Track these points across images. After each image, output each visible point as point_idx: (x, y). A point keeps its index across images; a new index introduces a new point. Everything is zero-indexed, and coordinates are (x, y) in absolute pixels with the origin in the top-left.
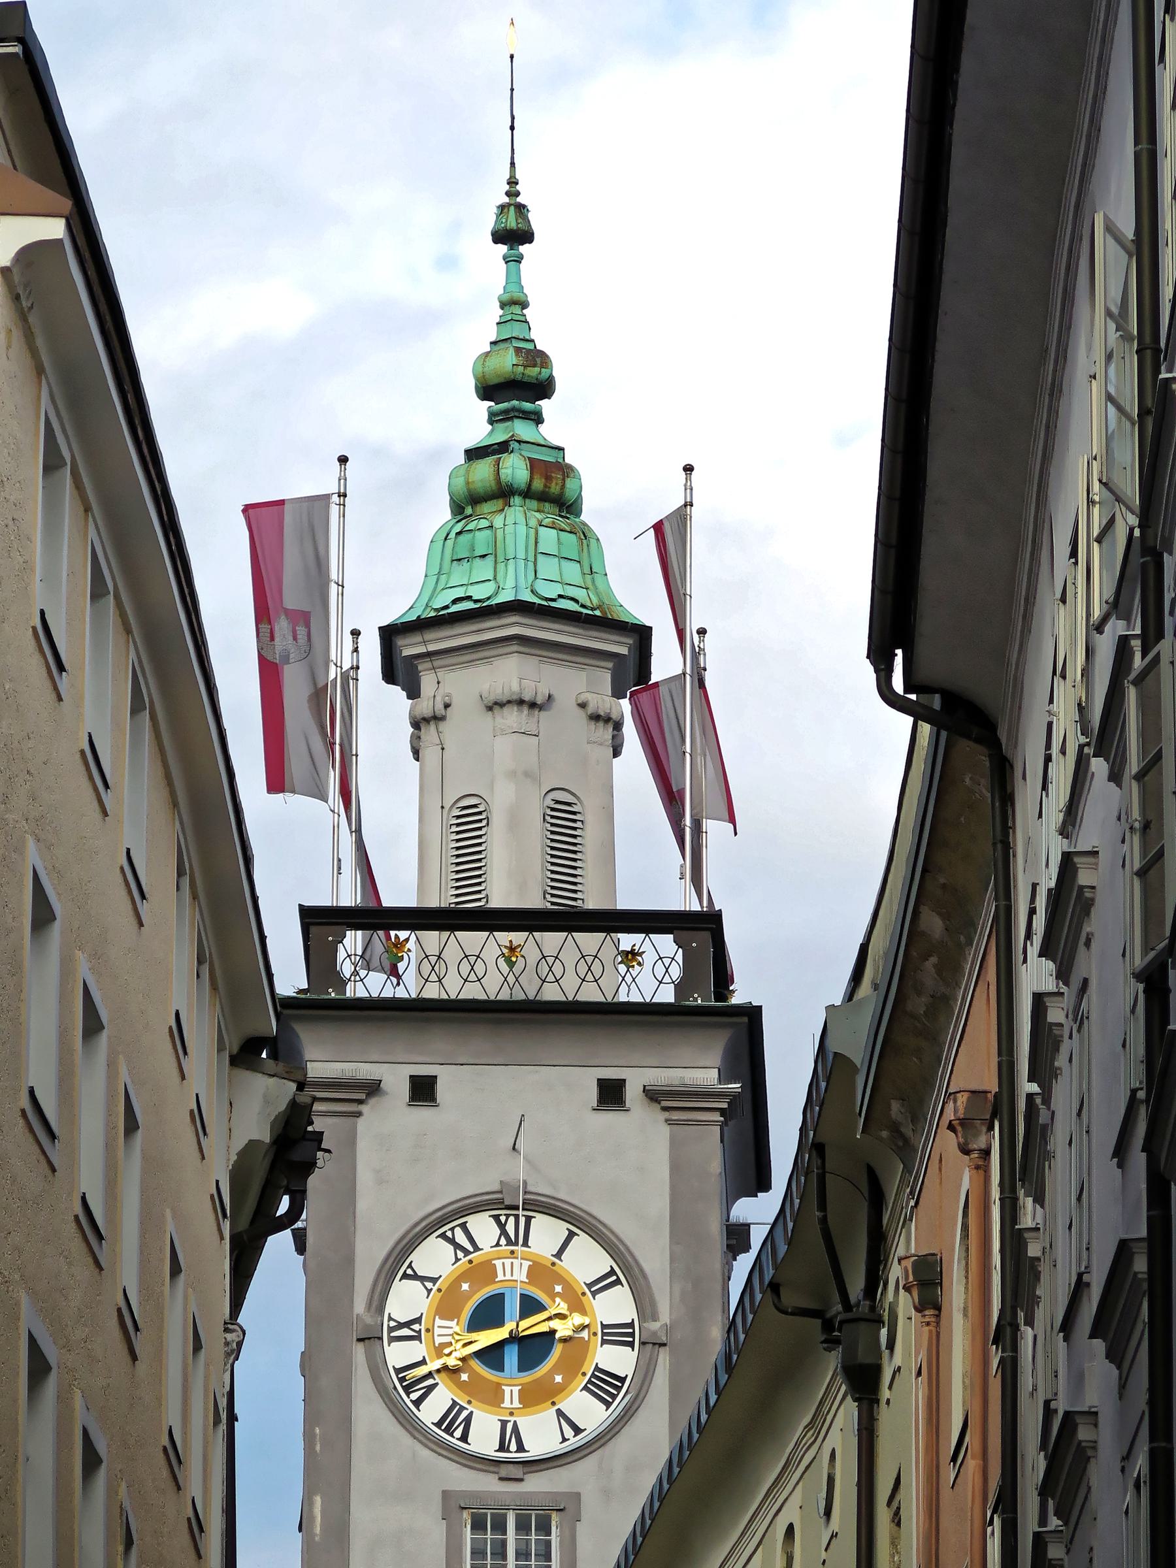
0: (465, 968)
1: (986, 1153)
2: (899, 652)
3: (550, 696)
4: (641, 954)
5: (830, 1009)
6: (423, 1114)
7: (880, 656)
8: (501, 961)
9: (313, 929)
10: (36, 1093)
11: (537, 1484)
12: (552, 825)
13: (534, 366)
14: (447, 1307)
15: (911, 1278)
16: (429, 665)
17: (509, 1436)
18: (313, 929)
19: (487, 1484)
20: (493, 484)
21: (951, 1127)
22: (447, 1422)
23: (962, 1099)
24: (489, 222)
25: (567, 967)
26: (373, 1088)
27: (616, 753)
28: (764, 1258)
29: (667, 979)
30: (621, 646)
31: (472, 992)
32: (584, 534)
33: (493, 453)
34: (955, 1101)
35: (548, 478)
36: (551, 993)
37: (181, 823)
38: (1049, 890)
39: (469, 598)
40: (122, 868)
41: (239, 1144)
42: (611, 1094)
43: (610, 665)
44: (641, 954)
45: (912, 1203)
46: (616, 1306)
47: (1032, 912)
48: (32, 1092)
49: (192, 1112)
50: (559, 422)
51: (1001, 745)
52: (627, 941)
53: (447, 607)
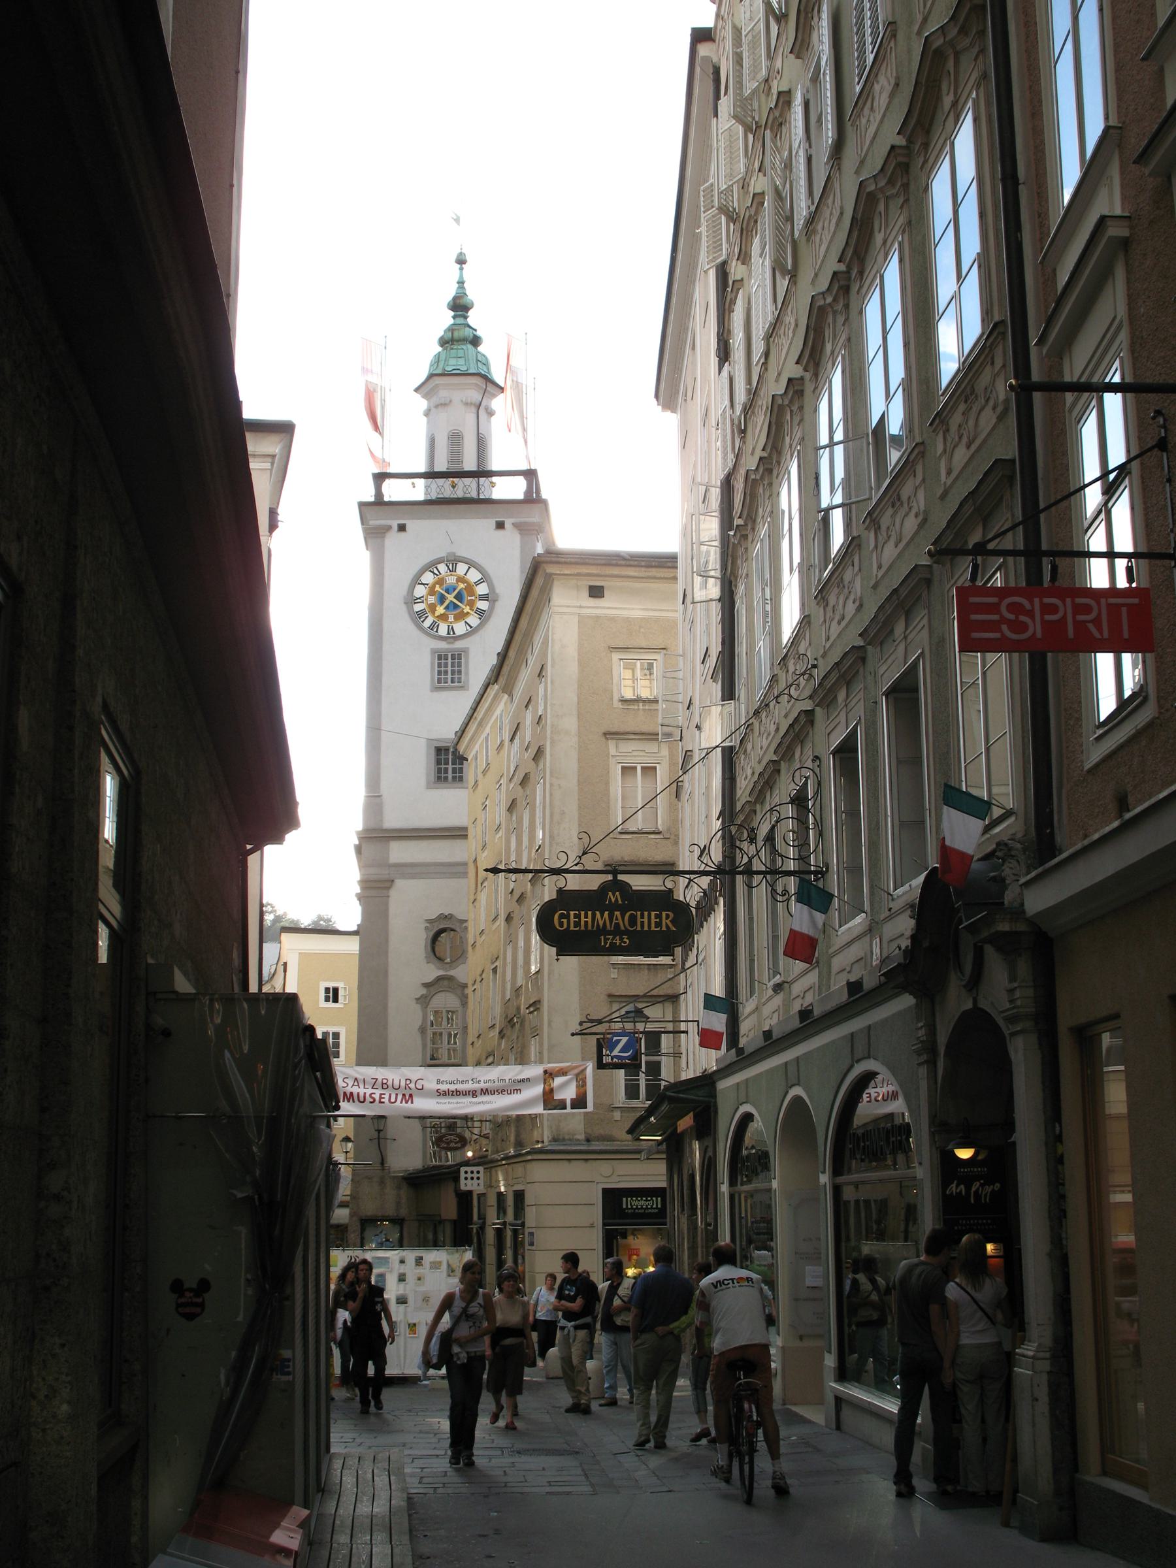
5: (362, 505)
6: (402, 534)
11: (459, 645)
14: (432, 592)
17: (451, 630)
19: (443, 645)
22: (431, 627)
24: (454, 257)
26: (389, 528)
42: (500, 526)
46: (482, 589)
50: (473, 318)
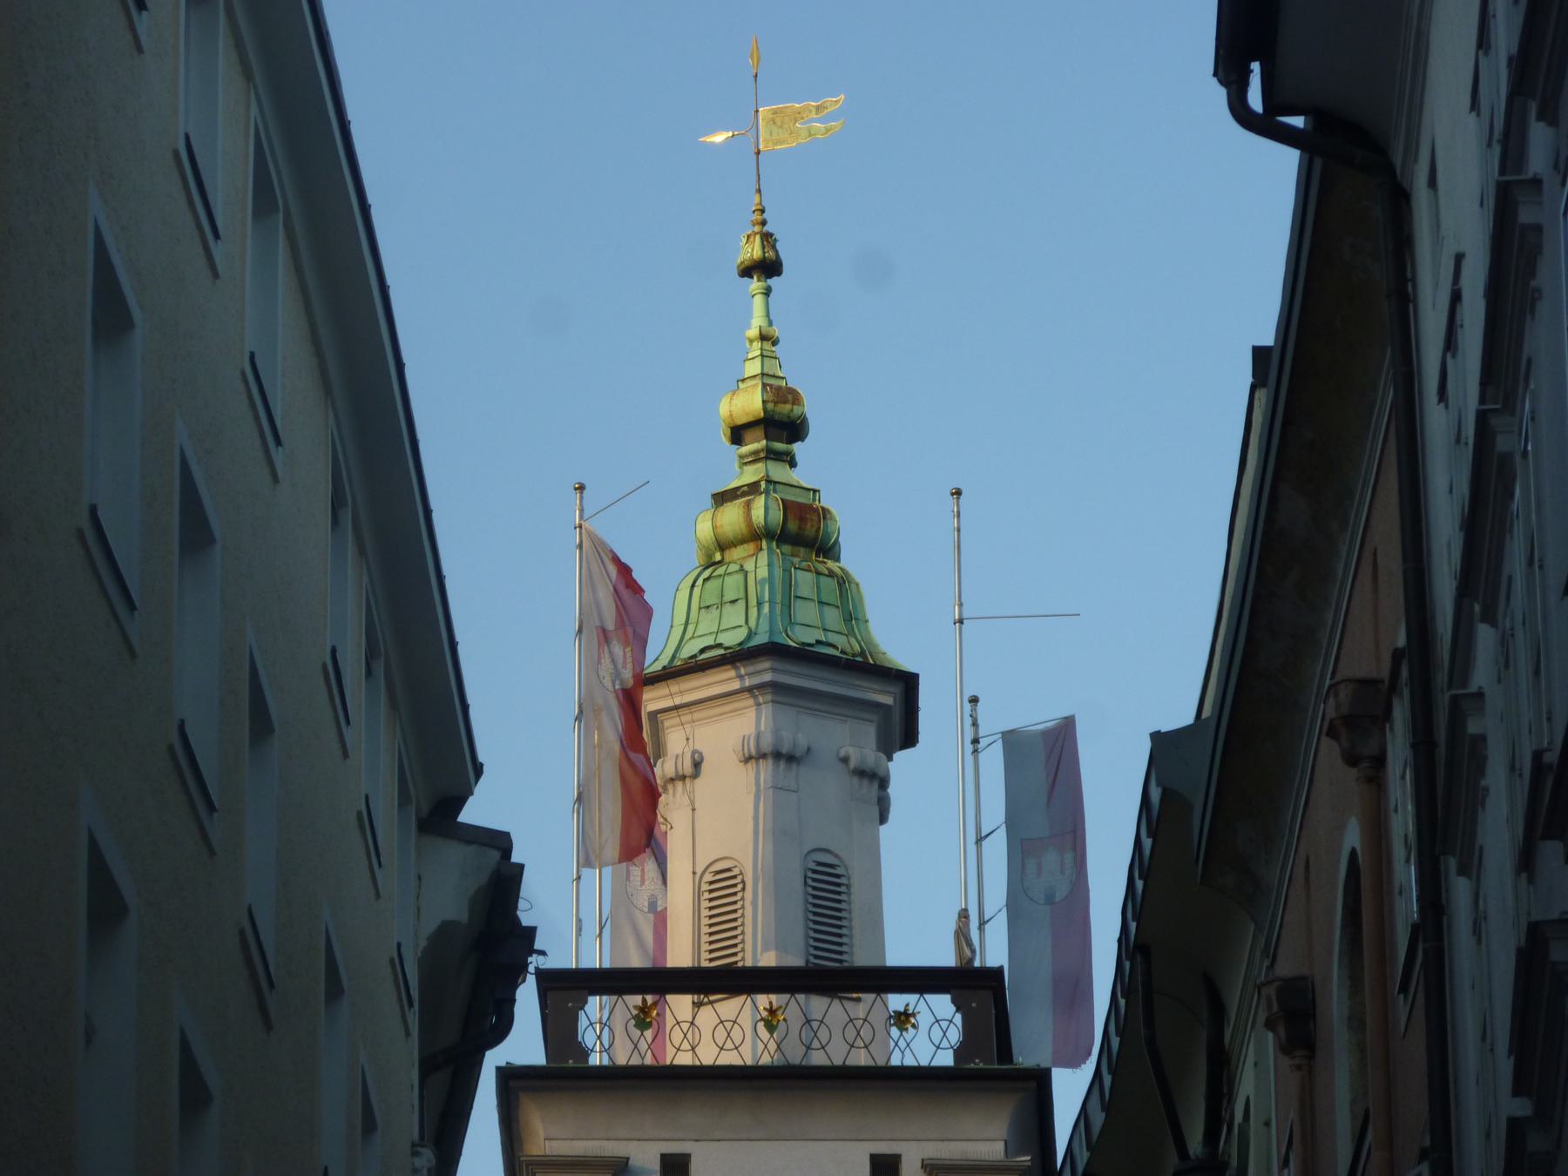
0: (721, 1034)
1: (1380, 761)
2: (1256, 66)
3: (809, 749)
4: (913, 1015)
7: (1230, 71)
8: (761, 1025)
9: (549, 994)
10: (99, 514)
12: (814, 888)
13: (785, 402)
15: (1275, 1008)
16: (677, 720)
18: (549, 994)
20: (743, 526)
21: (1332, 732)
23: (1345, 693)
25: (838, 1032)
27: (883, 819)
28: (1076, 1150)
29: (945, 1044)
30: (886, 697)
31: (729, 1059)
32: (844, 582)
33: (744, 494)
34: (1336, 695)
35: (802, 520)
36: (818, 1059)
37: (336, 415)
38: (1510, 59)
39: (719, 646)
40: (243, 374)
41: (430, 925)
43: (875, 718)
44: (913, 1015)
45: (1266, 963)
47: (1450, 344)
48: (93, 511)
49: (359, 814)
50: (814, 466)
51: (1394, 171)
52: (896, 1001)
53: (694, 656)
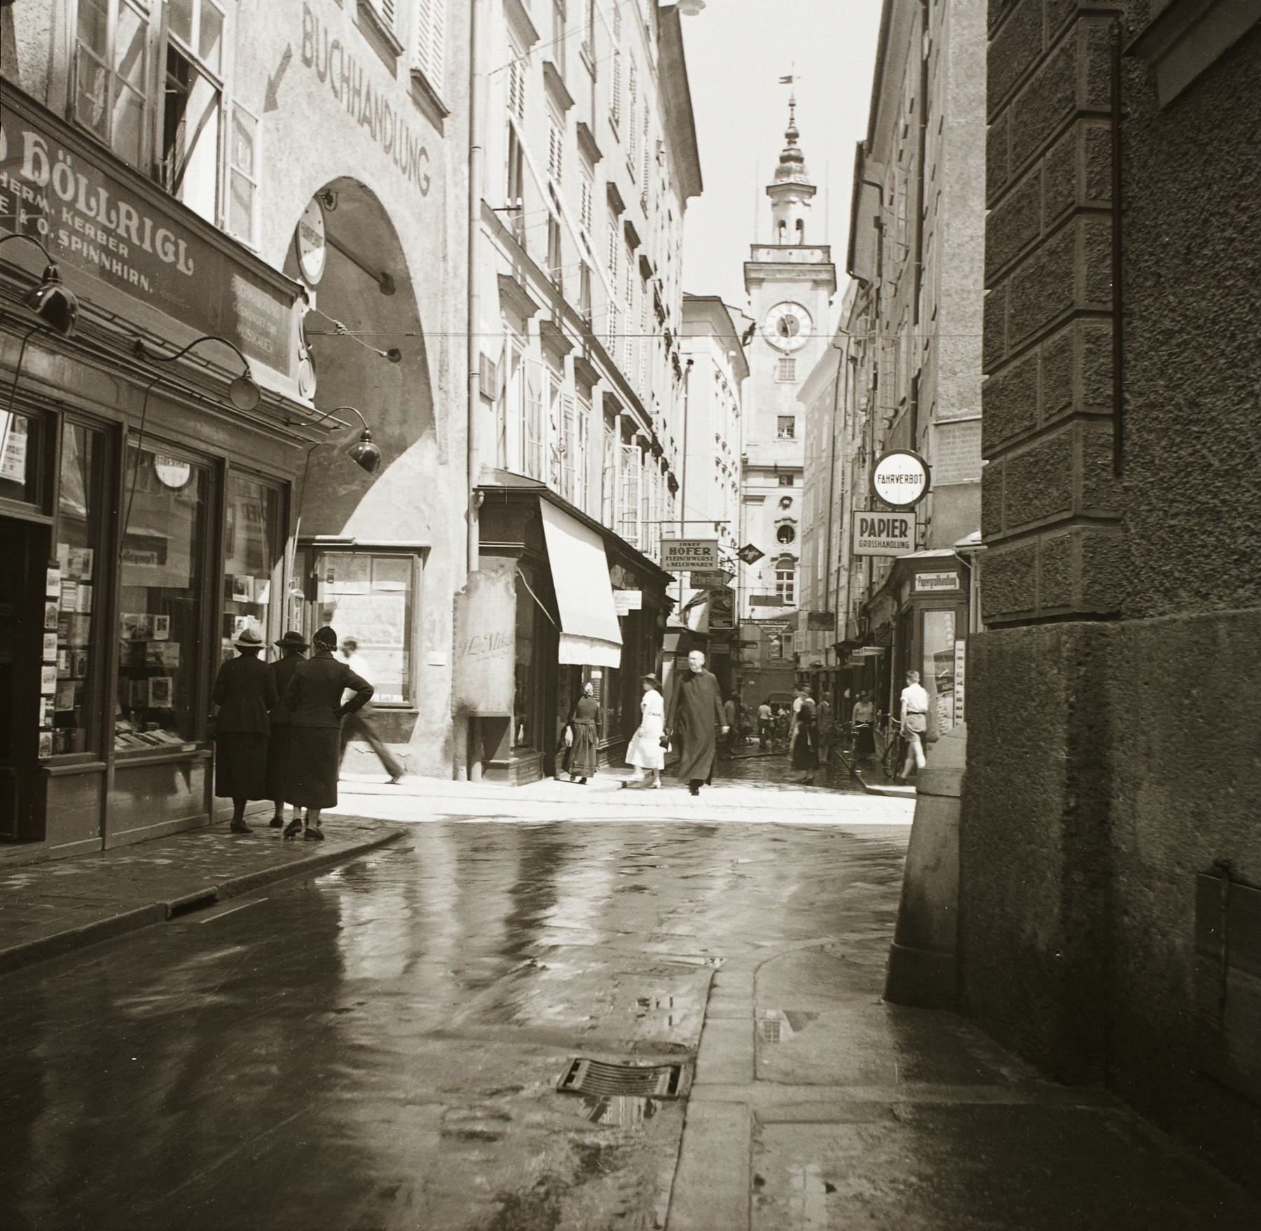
50: (800, 143)
